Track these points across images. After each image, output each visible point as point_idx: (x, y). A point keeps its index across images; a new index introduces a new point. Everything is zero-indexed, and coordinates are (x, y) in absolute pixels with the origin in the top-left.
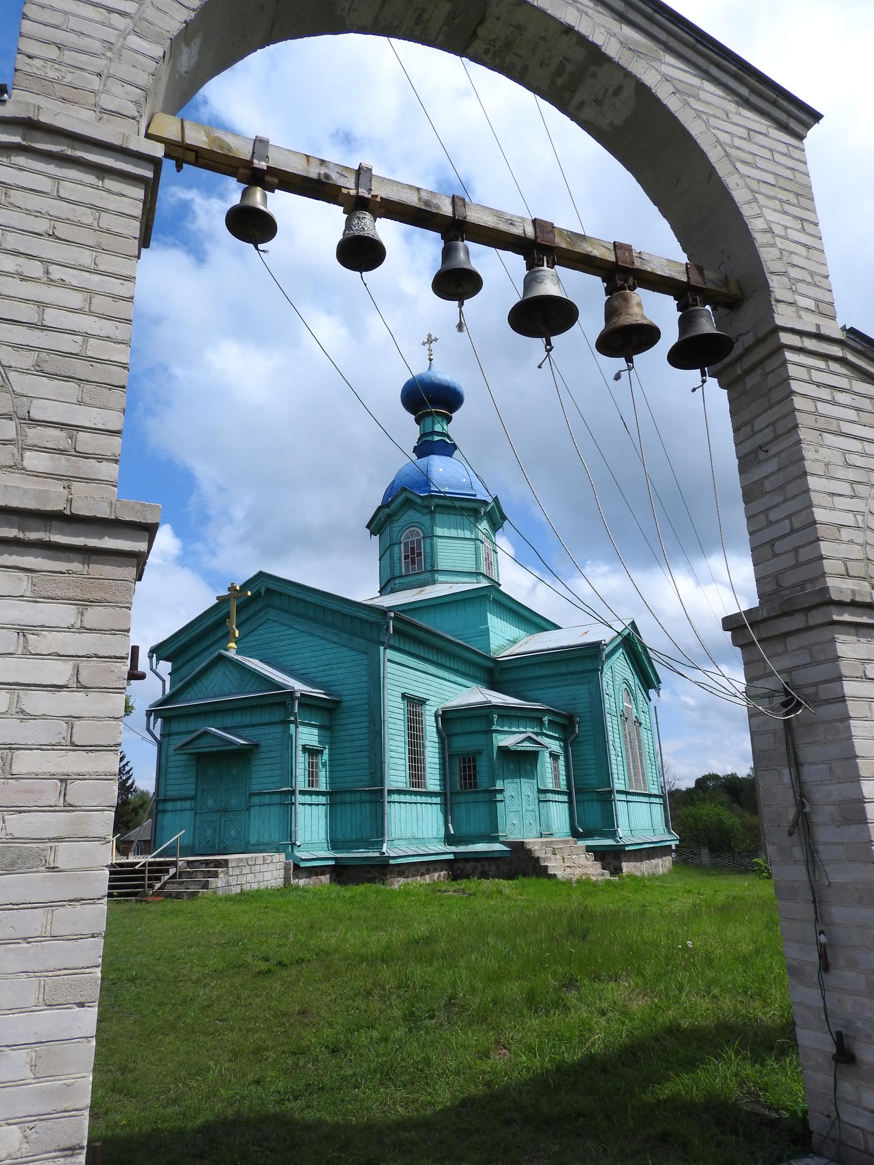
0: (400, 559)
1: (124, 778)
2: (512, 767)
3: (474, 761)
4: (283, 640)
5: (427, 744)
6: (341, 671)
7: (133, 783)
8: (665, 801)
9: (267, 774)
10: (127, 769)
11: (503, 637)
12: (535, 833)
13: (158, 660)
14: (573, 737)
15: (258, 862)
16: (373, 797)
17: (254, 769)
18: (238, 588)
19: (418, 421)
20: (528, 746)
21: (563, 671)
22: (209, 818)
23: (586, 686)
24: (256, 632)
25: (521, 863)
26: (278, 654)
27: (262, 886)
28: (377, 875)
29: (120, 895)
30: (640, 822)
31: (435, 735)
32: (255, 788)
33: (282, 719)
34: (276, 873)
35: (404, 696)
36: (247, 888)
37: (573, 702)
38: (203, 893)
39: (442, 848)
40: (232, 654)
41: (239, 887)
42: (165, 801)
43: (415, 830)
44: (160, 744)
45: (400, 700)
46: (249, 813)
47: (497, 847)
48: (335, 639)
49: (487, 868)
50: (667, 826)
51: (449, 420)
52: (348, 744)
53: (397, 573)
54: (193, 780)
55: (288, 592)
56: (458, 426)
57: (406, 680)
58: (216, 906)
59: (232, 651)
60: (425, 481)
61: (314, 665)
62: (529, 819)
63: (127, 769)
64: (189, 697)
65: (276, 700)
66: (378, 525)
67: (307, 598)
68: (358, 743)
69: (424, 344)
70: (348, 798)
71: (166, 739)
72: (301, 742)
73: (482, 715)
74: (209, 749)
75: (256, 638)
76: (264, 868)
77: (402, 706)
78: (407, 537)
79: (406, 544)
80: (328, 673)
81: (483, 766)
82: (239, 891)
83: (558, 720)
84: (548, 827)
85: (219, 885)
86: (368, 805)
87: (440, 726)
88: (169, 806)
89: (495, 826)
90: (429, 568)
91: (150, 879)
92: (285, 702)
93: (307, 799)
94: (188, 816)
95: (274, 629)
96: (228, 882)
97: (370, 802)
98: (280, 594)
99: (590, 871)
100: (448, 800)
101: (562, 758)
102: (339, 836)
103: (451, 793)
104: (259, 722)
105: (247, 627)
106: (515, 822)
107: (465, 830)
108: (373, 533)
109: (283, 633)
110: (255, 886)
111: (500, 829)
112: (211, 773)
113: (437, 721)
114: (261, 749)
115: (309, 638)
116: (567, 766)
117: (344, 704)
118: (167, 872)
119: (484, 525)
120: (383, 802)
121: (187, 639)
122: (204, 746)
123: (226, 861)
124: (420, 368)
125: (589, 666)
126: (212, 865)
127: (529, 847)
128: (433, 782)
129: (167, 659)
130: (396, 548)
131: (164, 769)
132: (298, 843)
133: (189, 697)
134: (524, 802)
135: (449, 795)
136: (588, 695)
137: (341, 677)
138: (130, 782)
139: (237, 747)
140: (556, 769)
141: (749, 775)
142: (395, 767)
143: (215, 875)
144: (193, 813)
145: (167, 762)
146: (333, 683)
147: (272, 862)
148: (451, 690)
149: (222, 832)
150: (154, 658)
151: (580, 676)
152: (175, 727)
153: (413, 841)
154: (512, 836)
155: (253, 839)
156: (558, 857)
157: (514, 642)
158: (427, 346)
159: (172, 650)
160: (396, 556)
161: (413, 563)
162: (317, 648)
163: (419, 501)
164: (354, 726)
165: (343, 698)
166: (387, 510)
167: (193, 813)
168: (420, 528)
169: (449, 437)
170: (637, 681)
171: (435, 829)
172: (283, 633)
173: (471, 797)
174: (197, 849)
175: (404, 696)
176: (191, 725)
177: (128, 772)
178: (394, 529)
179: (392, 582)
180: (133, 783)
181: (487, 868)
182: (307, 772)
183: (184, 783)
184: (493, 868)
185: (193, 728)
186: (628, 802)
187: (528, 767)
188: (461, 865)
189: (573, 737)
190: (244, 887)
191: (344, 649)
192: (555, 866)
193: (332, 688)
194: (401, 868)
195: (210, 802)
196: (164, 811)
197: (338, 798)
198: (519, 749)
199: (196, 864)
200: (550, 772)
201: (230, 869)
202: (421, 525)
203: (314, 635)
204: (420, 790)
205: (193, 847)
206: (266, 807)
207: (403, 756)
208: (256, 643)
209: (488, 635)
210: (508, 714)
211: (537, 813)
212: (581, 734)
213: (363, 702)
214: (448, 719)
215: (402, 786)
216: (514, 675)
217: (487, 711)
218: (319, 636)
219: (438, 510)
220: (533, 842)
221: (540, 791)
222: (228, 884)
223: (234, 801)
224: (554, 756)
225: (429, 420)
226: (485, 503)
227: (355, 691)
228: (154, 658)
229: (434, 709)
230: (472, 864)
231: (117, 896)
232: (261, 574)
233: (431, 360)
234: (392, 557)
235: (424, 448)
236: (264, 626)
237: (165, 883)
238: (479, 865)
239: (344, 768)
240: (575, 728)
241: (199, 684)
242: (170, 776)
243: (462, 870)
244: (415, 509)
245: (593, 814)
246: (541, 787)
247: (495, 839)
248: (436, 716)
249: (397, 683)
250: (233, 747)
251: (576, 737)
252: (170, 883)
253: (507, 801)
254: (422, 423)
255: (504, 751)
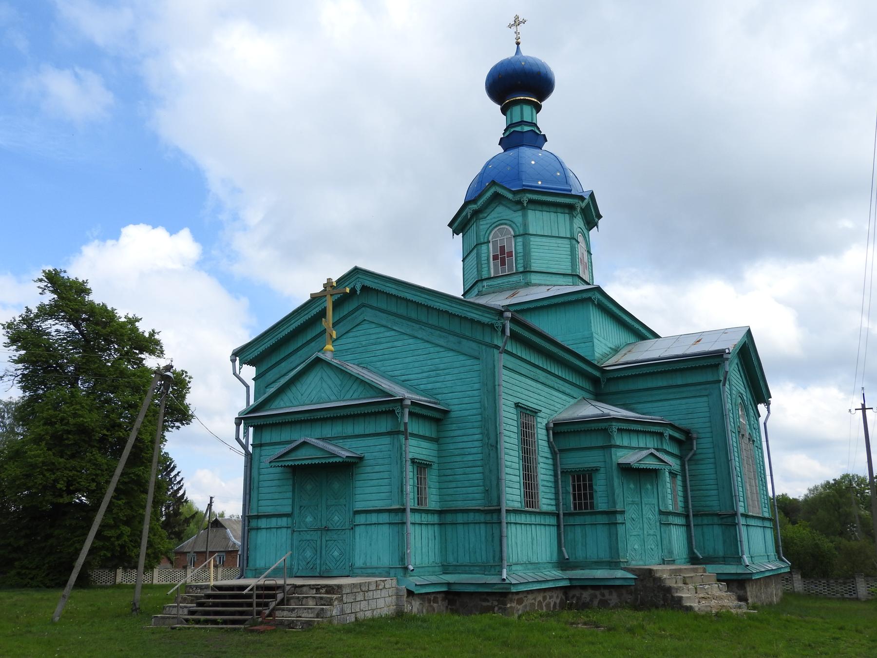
0: (488, 259)
1: (175, 488)
2: (632, 486)
3: (591, 480)
4: (381, 343)
5: (541, 460)
6: (448, 377)
7: (184, 494)
8: (775, 525)
9: (374, 489)
10: (178, 479)
11: (606, 345)
12: (657, 559)
13: (241, 364)
14: (691, 454)
15: (371, 588)
16: (488, 518)
17: (358, 484)
18: (335, 284)
19: (504, 111)
20: (651, 464)
21: (679, 382)
22: (308, 537)
23: (705, 399)
24: (351, 334)
25: (649, 594)
26: (374, 359)
27: (376, 614)
28: (496, 603)
29: (225, 622)
30: (759, 549)
31: (547, 449)
32: (359, 506)
33: (389, 430)
34: (388, 600)
35: (517, 405)
36: (361, 616)
37: (690, 416)
38: (318, 622)
39: (558, 574)
40: (328, 357)
41: (353, 615)
42: (258, 517)
43: (530, 554)
44: (248, 455)
45: (513, 411)
46: (354, 533)
47: (620, 574)
48: (441, 342)
49: (607, 596)
50: (777, 551)
51: (538, 108)
52: (458, 459)
53: (485, 275)
54: (289, 495)
55: (387, 290)
56: (550, 117)
57: (518, 389)
58: (340, 639)
59: (328, 351)
60: (517, 171)
61: (416, 370)
62: (651, 544)
63: (178, 479)
64: (282, 404)
65: (383, 408)
66: (461, 224)
67: (409, 297)
68: (470, 458)
69: (510, 26)
70: (460, 518)
71: (258, 450)
72: (410, 456)
73: (600, 427)
74: (310, 462)
75: (351, 340)
76: (377, 594)
77: (515, 417)
78: (495, 236)
79: (495, 243)
80: (434, 379)
81: (600, 484)
82: (353, 620)
83: (676, 435)
84: (670, 552)
85: (334, 613)
86: (483, 526)
87: (552, 440)
88: (263, 523)
89: (614, 548)
90: (521, 270)
91: (258, 605)
92: (394, 411)
93: (417, 518)
94: (284, 534)
95: (371, 331)
96: (342, 610)
97: (486, 523)
98: (377, 292)
99: (726, 602)
100: (562, 520)
101: (679, 478)
102: (451, 559)
103: (564, 514)
104: (362, 432)
105: (343, 328)
106: (636, 547)
107: (580, 555)
108: (456, 232)
109: (381, 335)
110: (369, 614)
111: (621, 554)
112: (309, 487)
113: (548, 435)
114: (365, 462)
115: (411, 341)
116: (685, 486)
117: (453, 414)
118: (274, 597)
119: (579, 222)
120: (500, 523)
121: (273, 341)
122: (304, 457)
123: (340, 587)
124: (503, 52)
125: (709, 377)
126: (323, 591)
127: (658, 575)
128: (545, 502)
129: (251, 363)
130: (484, 247)
131: (256, 485)
132: (411, 567)
133: (282, 404)
134: (645, 526)
135: (562, 516)
136: (707, 409)
137: (449, 384)
138: (181, 492)
139: (341, 460)
140: (674, 491)
141: (806, 496)
142: (510, 484)
143: (330, 603)
144: (289, 531)
145: (259, 474)
146: (440, 391)
147: (384, 587)
148: (559, 401)
149: (324, 552)
150: (237, 362)
151: (699, 387)
152: (267, 437)
153: (530, 566)
154: (633, 563)
155: (359, 562)
156: (691, 586)
157: (616, 350)
158: (514, 29)
159: (256, 353)
160: (484, 257)
161: (503, 263)
162: (420, 352)
163: (510, 196)
164: (465, 439)
165: (452, 407)
166: (474, 207)
167: (289, 531)
168: (510, 226)
169: (538, 129)
170: (749, 396)
171: (548, 554)
172: (381, 335)
173: (588, 519)
174: (295, 570)
175: (517, 405)
176: (285, 435)
177: (179, 482)
178: (481, 227)
179: (479, 284)
180: (184, 494)
181: (607, 596)
182: (416, 489)
183: (277, 497)
184: (614, 598)
185: (288, 439)
186: (747, 526)
187: (649, 487)
188: (577, 593)
189: (691, 454)
190: (358, 615)
191: (451, 354)
192: (687, 595)
193: (439, 397)
194: (520, 596)
195: (309, 519)
196: (258, 529)
197: (449, 518)
198: (641, 467)
199: (305, 589)
200: (670, 493)
201: (345, 596)
202: (511, 223)
203: (416, 338)
204: (531, 509)
205: (291, 569)
206: (373, 527)
207: (517, 472)
208: (350, 346)
209: (592, 342)
210: (629, 427)
211: (659, 537)
212: (699, 451)
213: (475, 411)
214: (560, 430)
215: (517, 505)
216: (622, 386)
217: (605, 424)
218: (422, 339)
219: (530, 206)
220: (663, 571)
221: (661, 513)
222: (342, 612)
223: (336, 518)
224: (673, 475)
225: (516, 110)
226: (582, 198)
227: (466, 400)
228: (237, 362)
229: (545, 422)
230: (590, 591)
231: (222, 624)
232: (356, 271)
233: (518, 44)
234: (478, 256)
235: (510, 141)
236: (359, 328)
237: (274, 609)
238: (598, 593)
239: (453, 485)
240: (692, 444)
241: (294, 389)
242: (262, 490)
243: (579, 599)
244: (504, 205)
245: (713, 539)
246: (663, 509)
247: (613, 564)
248: (547, 429)
249: (510, 392)
250: (337, 460)
251: (694, 455)
252: (280, 609)
253: (628, 525)
254: (508, 113)
255: (627, 470)
